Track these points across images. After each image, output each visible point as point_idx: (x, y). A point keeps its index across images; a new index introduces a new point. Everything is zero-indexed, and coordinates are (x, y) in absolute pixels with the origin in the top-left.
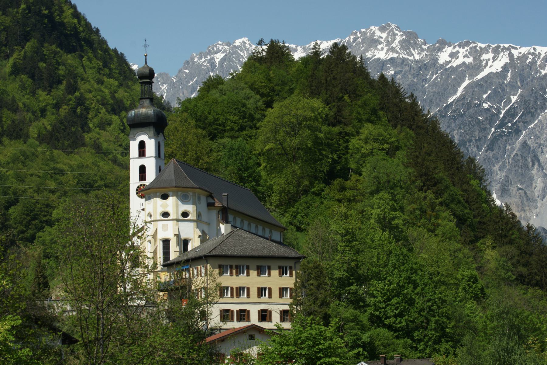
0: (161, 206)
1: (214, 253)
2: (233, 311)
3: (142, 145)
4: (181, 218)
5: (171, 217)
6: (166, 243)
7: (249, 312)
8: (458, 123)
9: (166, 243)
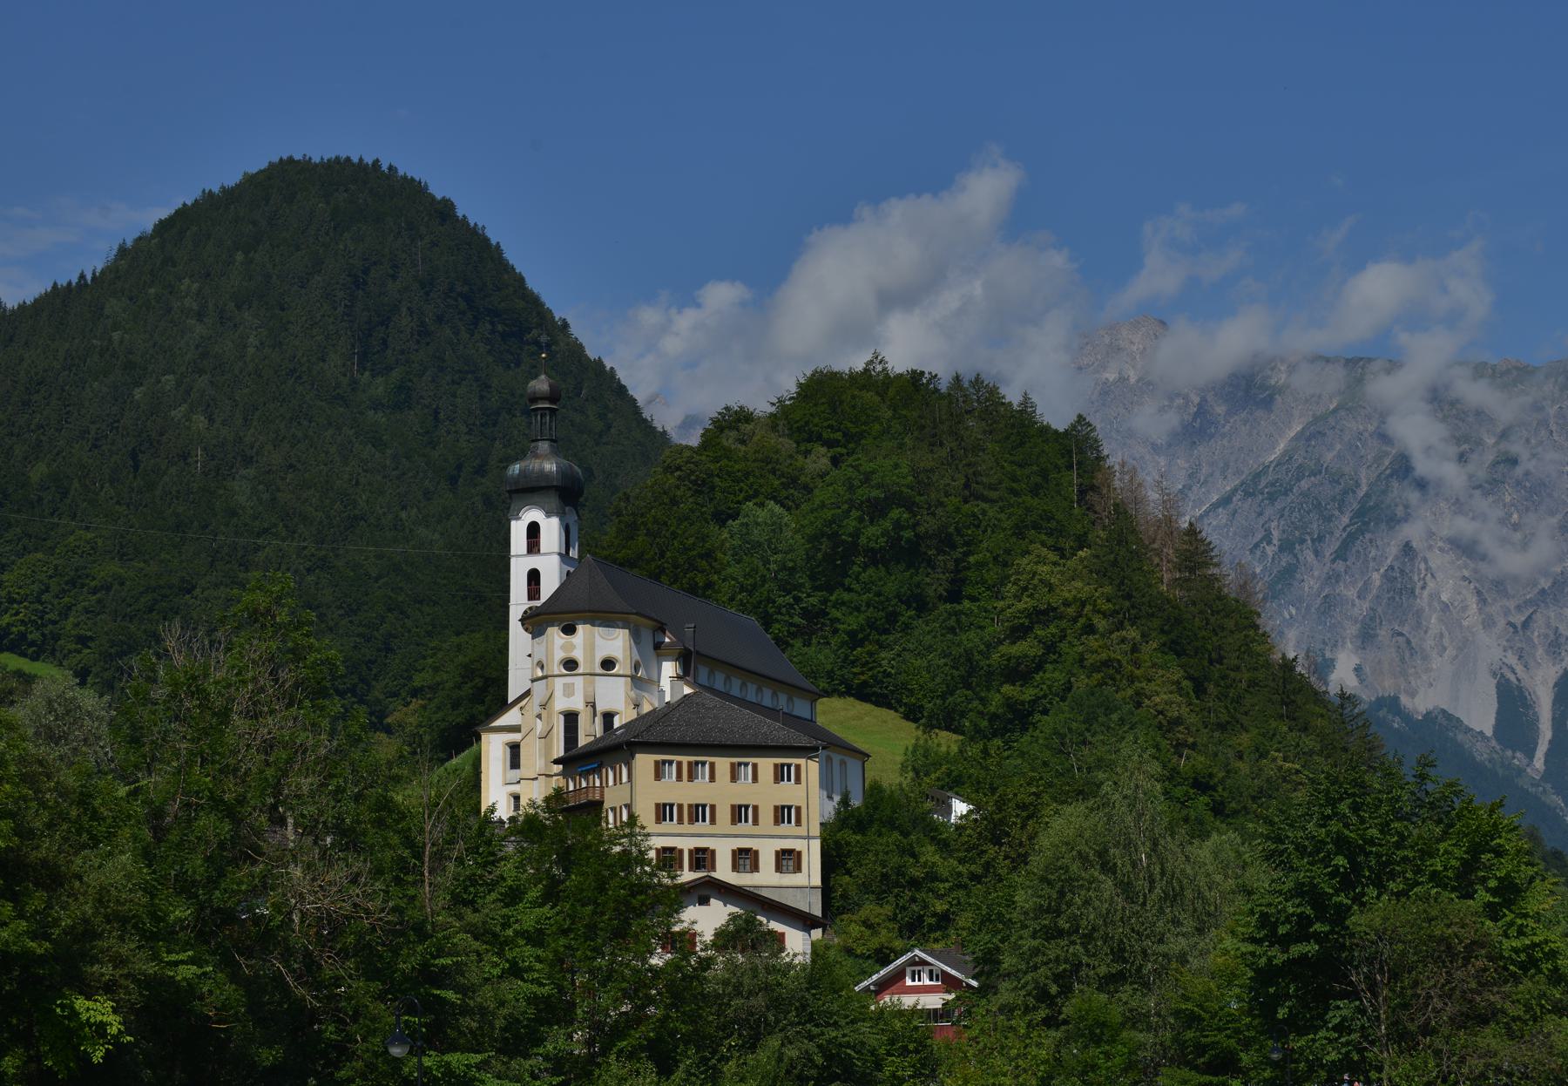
0: (562, 647)
1: (645, 738)
2: (681, 851)
3: (533, 530)
4: (599, 670)
5: (580, 670)
6: (571, 719)
7: (713, 852)
8: (1278, 505)
9: (571, 719)
